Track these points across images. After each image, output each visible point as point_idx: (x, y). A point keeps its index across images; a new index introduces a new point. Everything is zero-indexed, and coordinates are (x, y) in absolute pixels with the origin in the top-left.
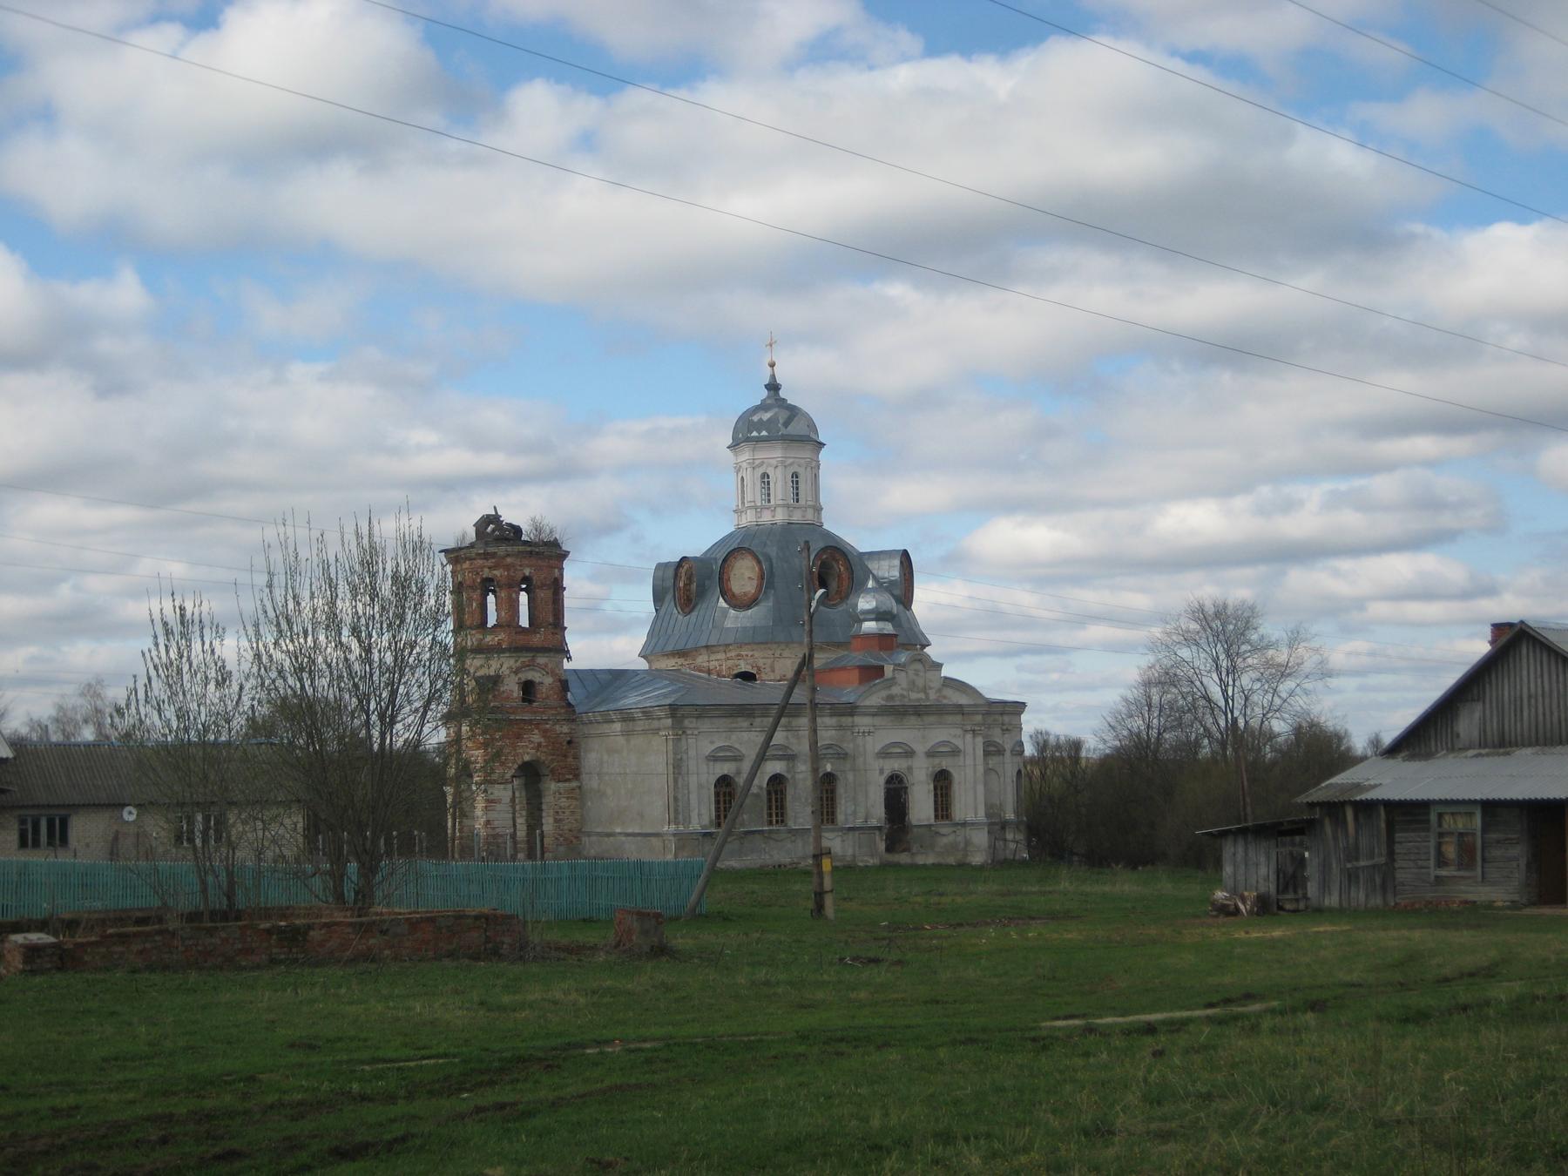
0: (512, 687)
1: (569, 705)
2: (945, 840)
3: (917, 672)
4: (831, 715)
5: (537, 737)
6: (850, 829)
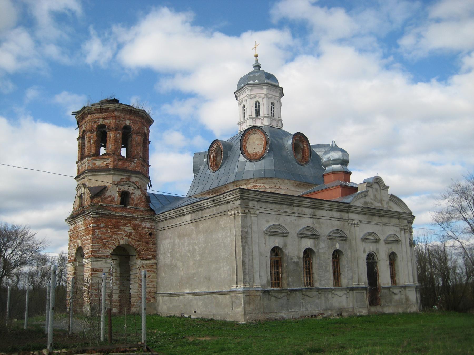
0: (114, 194)
1: (151, 210)
2: (396, 297)
3: (376, 190)
4: (338, 211)
5: (129, 229)
6: (352, 289)
